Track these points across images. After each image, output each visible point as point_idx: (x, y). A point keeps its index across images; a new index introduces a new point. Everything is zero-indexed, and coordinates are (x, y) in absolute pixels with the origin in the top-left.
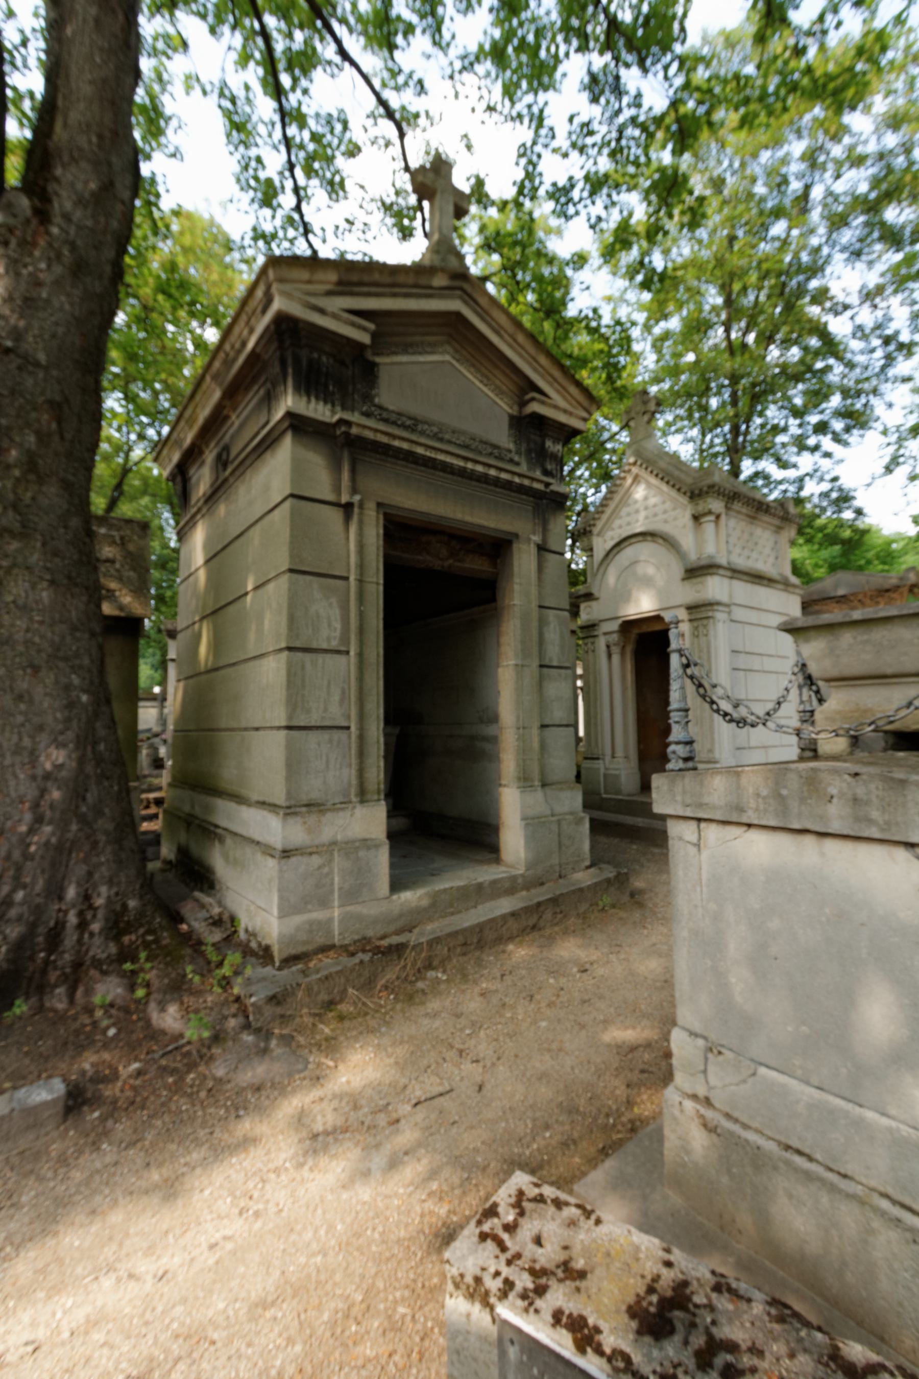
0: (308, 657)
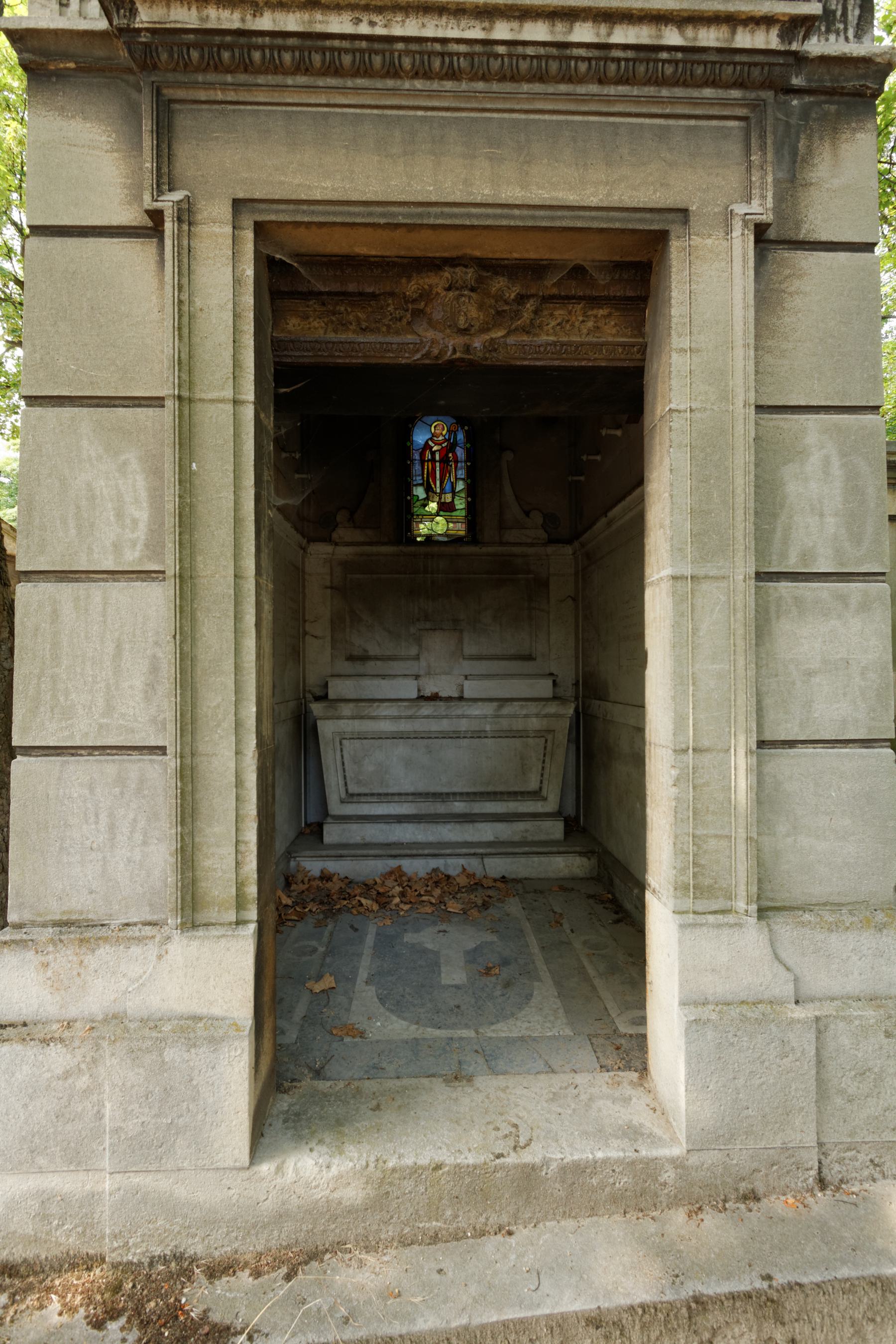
0: (66, 591)
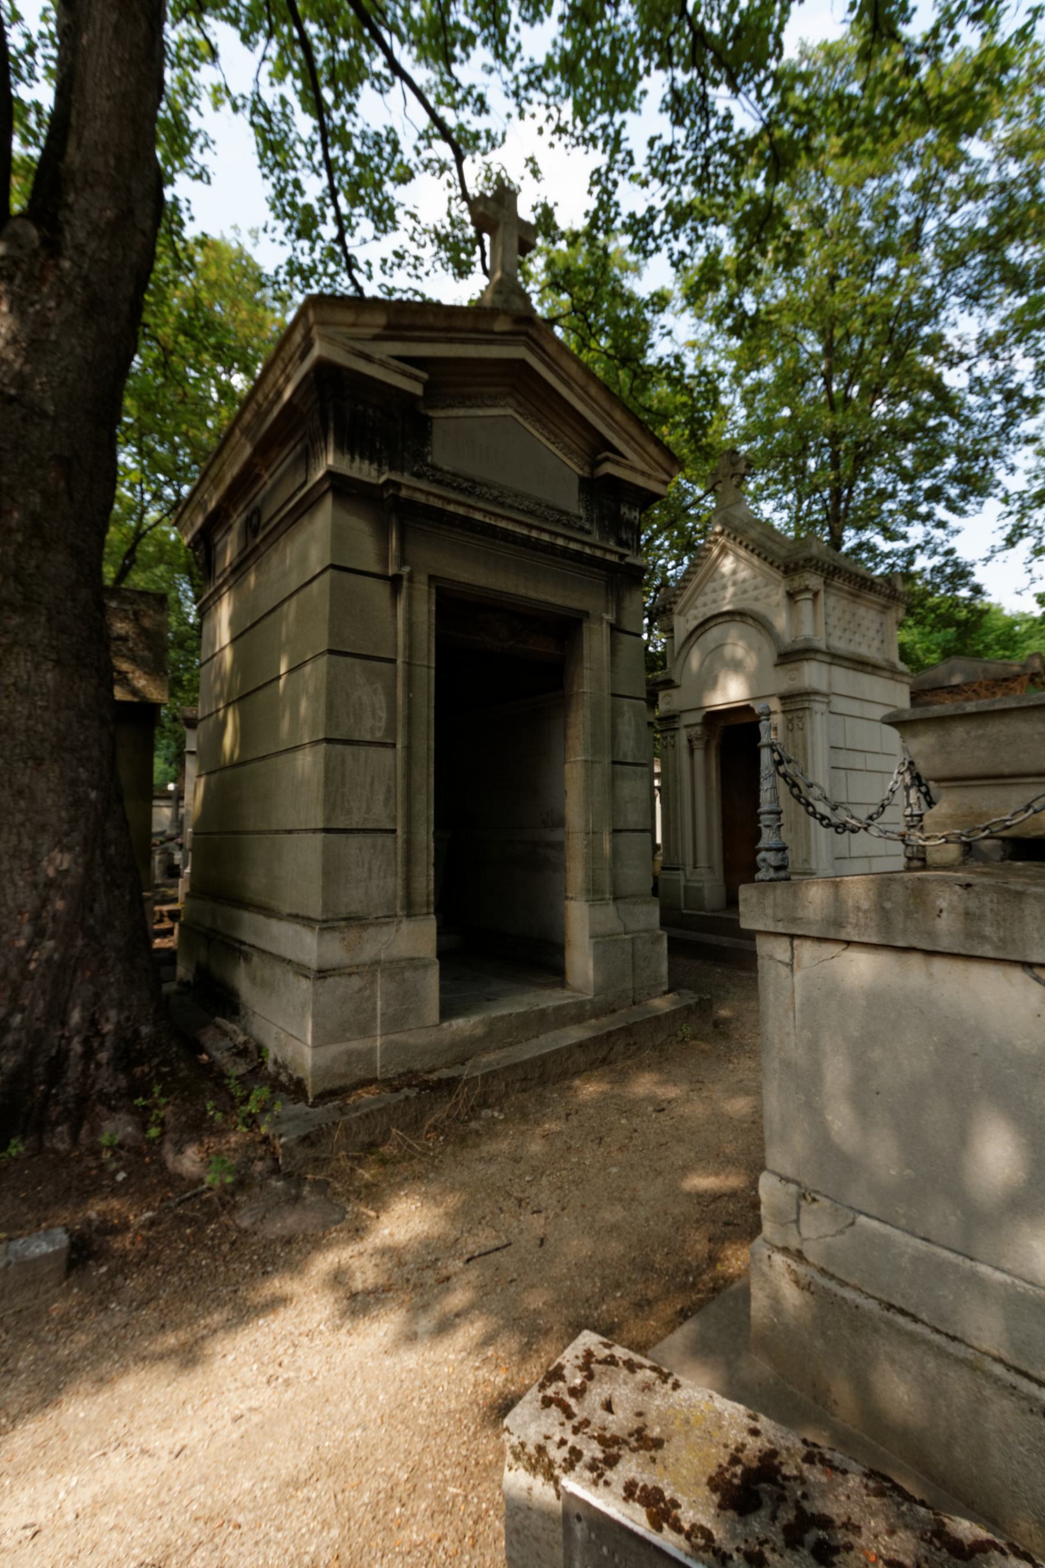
0: (348, 750)
